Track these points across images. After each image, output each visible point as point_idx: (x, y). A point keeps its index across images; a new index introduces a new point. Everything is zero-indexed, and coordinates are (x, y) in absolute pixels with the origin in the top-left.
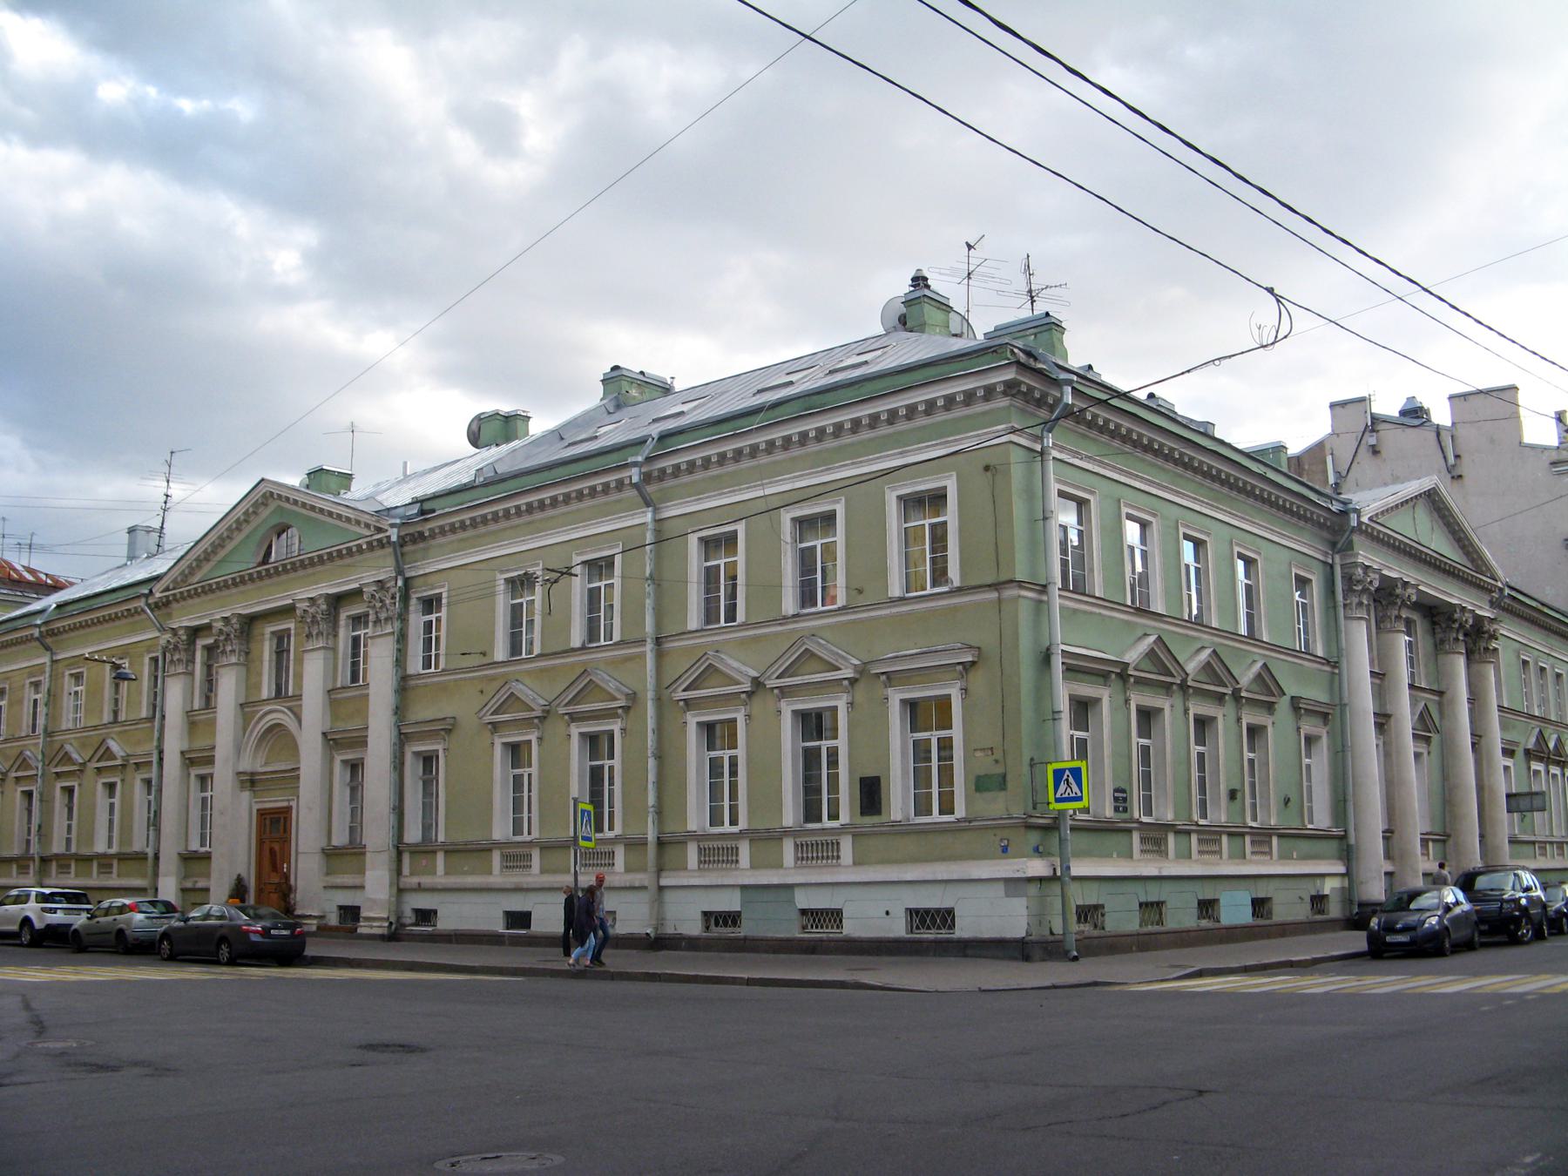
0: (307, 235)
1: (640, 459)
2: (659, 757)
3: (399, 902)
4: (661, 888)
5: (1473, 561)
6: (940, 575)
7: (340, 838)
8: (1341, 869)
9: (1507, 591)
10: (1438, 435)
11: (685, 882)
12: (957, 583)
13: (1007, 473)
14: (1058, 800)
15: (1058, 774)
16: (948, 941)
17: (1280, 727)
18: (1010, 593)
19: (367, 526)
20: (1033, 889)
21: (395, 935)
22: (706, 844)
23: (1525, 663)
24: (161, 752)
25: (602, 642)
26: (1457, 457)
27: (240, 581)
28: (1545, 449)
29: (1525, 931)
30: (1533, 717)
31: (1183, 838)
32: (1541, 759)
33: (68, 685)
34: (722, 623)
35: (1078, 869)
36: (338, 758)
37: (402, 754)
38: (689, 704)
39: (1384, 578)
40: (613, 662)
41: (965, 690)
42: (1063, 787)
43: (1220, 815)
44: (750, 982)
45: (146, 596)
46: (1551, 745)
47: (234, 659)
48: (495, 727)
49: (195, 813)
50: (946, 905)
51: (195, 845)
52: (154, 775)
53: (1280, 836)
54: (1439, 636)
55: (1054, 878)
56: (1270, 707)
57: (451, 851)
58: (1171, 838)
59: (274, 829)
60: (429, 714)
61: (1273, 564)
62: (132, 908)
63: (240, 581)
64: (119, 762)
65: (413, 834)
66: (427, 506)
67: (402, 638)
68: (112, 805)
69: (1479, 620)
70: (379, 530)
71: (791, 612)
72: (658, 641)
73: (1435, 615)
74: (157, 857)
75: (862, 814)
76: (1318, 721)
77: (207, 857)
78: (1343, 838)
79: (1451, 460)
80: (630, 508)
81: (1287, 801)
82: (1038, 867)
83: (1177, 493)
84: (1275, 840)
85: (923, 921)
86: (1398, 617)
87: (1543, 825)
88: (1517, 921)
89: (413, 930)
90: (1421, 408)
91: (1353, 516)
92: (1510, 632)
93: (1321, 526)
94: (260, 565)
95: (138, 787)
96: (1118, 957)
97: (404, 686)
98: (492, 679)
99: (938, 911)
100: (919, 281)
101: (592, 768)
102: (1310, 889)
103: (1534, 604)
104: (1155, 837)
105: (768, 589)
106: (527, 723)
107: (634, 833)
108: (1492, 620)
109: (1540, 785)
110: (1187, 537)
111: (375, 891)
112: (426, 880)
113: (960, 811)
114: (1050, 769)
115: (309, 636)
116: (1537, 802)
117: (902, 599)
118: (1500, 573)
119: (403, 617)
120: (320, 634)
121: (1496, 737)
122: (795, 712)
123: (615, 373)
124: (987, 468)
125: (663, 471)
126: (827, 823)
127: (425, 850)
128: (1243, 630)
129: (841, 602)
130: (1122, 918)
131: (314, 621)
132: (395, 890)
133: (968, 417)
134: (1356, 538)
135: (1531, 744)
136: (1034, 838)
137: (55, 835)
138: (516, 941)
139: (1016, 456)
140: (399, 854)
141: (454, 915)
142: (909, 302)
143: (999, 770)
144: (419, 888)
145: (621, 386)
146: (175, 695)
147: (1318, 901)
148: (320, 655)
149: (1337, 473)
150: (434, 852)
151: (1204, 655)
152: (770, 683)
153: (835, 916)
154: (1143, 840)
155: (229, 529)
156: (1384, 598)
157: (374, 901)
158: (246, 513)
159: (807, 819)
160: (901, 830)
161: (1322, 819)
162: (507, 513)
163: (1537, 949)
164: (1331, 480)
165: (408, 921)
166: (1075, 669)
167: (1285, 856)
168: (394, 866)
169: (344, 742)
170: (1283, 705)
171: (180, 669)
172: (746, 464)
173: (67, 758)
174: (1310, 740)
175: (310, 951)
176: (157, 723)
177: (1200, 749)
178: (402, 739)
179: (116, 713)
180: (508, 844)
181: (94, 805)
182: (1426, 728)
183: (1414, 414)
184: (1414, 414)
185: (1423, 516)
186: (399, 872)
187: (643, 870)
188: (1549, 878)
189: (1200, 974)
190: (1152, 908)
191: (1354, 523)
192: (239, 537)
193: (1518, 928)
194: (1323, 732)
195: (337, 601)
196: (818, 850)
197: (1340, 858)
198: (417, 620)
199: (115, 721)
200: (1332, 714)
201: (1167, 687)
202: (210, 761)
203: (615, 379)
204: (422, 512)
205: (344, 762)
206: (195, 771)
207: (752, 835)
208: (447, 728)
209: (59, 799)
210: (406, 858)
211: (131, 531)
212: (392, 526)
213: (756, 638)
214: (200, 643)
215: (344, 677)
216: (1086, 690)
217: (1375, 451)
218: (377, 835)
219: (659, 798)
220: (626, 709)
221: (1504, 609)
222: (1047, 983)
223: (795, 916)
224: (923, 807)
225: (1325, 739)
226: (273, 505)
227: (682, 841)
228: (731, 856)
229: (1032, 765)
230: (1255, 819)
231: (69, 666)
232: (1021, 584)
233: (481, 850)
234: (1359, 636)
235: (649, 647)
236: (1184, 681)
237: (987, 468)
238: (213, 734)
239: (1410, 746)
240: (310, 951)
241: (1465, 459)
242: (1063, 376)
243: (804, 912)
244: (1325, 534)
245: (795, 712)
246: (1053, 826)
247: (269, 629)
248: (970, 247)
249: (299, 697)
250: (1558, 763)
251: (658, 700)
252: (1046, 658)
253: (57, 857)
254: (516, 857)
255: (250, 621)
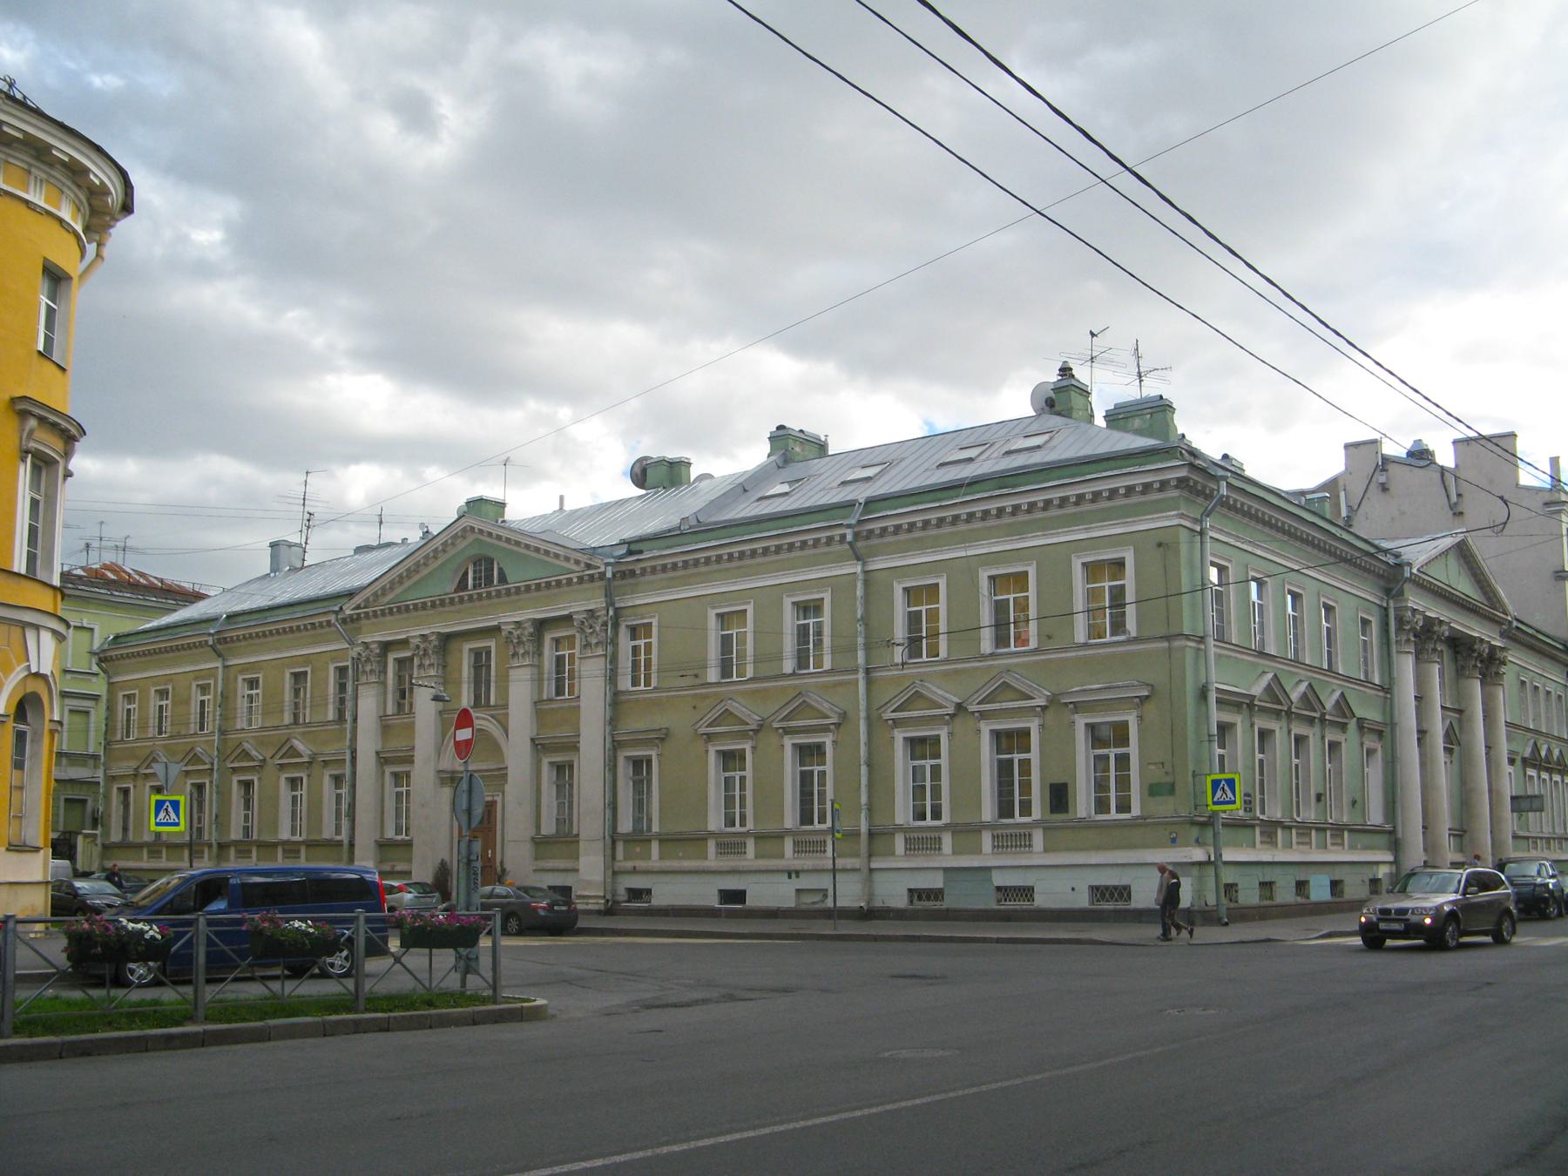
0: (229, 207)
1: (853, 522)
2: (869, 765)
3: (614, 883)
4: (871, 870)
5: (1489, 599)
6: (1118, 625)
7: (548, 828)
8: (1391, 858)
9: (1515, 624)
10: (1442, 475)
11: (894, 865)
12: (1134, 634)
13: (1177, 552)
14: (1215, 803)
15: (1216, 784)
16: (1127, 911)
17: (1350, 742)
18: (1177, 643)
19: (577, 562)
20: (1195, 871)
21: (610, 910)
22: (800, 838)
23: (1523, 683)
24: (354, 752)
25: (812, 670)
26: (1459, 495)
27: (438, 604)
28: (1539, 490)
29: (1553, 910)
30: (1528, 730)
31: (1321, 834)
32: (1534, 766)
33: (243, 690)
34: (925, 658)
35: (1228, 855)
36: (545, 761)
37: (615, 758)
38: (896, 723)
39: (1427, 618)
40: (825, 687)
41: (1140, 718)
42: (1219, 793)
43: (1310, 814)
44: (998, 941)
45: (336, 613)
46: (1543, 753)
47: (432, 672)
48: (709, 737)
49: (390, 804)
50: (1124, 882)
51: (390, 833)
52: (348, 770)
53: (1351, 831)
54: (1461, 663)
55: (1209, 863)
56: (1343, 727)
57: (664, 840)
58: (1279, 831)
59: (480, 825)
60: (641, 725)
61: (1347, 612)
62: (400, 889)
63: (438, 604)
64: (306, 759)
65: (625, 826)
66: (634, 547)
67: (614, 659)
68: (339, 797)
69: (1493, 648)
70: (589, 566)
71: (988, 651)
72: (868, 671)
73: (1459, 646)
74: (352, 845)
75: (1052, 811)
76: (1375, 737)
77: (408, 845)
78: (1392, 832)
79: (1454, 498)
80: (839, 559)
81: (1354, 803)
82: (1198, 854)
83: (1285, 557)
84: (1346, 834)
85: (1103, 895)
86: (1434, 650)
87: (1538, 824)
88: (1545, 901)
89: (629, 909)
90: (1427, 451)
91: (1407, 569)
92: (1516, 658)
93: (1380, 576)
94: (456, 591)
95: (327, 783)
96: (1269, 922)
97: (617, 701)
98: (706, 696)
99: (1116, 888)
100: (1065, 371)
101: (802, 773)
102: (1368, 874)
103: (1530, 631)
104: (1270, 829)
105: (965, 632)
106: (743, 735)
107: (845, 824)
108: (1502, 649)
109: (1534, 789)
110: (1213, 564)
111: (589, 875)
112: (641, 864)
113: (1136, 810)
114: (1209, 779)
115: (515, 655)
116: (1536, 804)
117: (1085, 645)
118: (1510, 608)
119: (614, 642)
120: (526, 653)
121: (1504, 748)
122: (992, 731)
123: (781, 432)
124: (1160, 545)
125: (871, 532)
126: (1018, 819)
127: (639, 838)
128: (1325, 666)
129: (1033, 644)
130: (1249, 896)
131: (520, 642)
132: (610, 872)
133: (1144, 503)
134: (1407, 587)
135: (1527, 753)
136: (1195, 832)
137: (233, 823)
138: (731, 914)
139: (1183, 535)
140: (614, 842)
141: (666, 893)
142: (1058, 389)
143: (1169, 779)
144: (634, 871)
145: (791, 447)
146: (368, 705)
147: (1375, 882)
148: (528, 671)
149: (1349, 507)
150: (649, 841)
151: (1303, 687)
152: (972, 708)
153: (1027, 892)
154: (1262, 833)
155: (427, 557)
156: (1425, 636)
157: (589, 883)
158: (445, 544)
159: (1001, 816)
160: (1085, 825)
161: (1376, 817)
162: (719, 558)
163: (1559, 922)
164: (1344, 513)
165: (621, 898)
166: (1227, 701)
167: (1352, 847)
168: (609, 852)
169: (554, 749)
170: (1352, 724)
171: (373, 679)
172: (947, 530)
173: (246, 755)
174: (1370, 752)
175: (581, 924)
176: (348, 726)
177: (1221, 751)
178: (615, 746)
179: (296, 716)
180: (721, 834)
181: (277, 796)
182: (1454, 739)
183: (1421, 455)
184: (1421, 455)
185: (1453, 562)
186: (614, 857)
187: (858, 856)
188: (1561, 866)
189: (1329, 935)
190: (1230, 888)
191: (1407, 575)
192: (434, 565)
193: (1547, 906)
194: (1378, 746)
195: (541, 625)
196: (1020, 840)
197: (1389, 849)
198: (625, 644)
199: (296, 722)
200: (1385, 731)
201: (1278, 713)
202: (409, 760)
203: (782, 438)
204: (630, 553)
205: (551, 763)
206: (388, 770)
207: (954, 828)
208: (662, 737)
209: (236, 792)
210: (620, 847)
211: (273, 545)
212: (607, 564)
213: (956, 671)
214: (391, 657)
215: (549, 689)
216: (1227, 717)
217: (1384, 488)
218: (590, 825)
219: (870, 797)
220: (838, 725)
221: (1510, 638)
222: (1263, 937)
223: (993, 892)
224: (1102, 806)
225: (1379, 753)
226: (471, 538)
227: (890, 833)
228: (934, 845)
229: (1194, 776)
230: (1263, 812)
231: (242, 672)
232: (1187, 637)
233: (697, 840)
234: (1406, 666)
235: (861, 675)
236: (1323, 715)
237: (1160, 545)
238: (412, 737)
239: (1441, 756)
240: (581, 924)
241: (1467, 496)
242: (1220, 473)
243: (999, 889)
244: (1382, 583)
245: (992, 731)
246: (1209, 822)
247: (467, 646)
248: (1093, 335)
249: (506, 706)
250: (1559, 772)
251: (868, 718)
252: (1203, 694)
253: (236, 843)
254: (732, 845)
255: (446, 639)
